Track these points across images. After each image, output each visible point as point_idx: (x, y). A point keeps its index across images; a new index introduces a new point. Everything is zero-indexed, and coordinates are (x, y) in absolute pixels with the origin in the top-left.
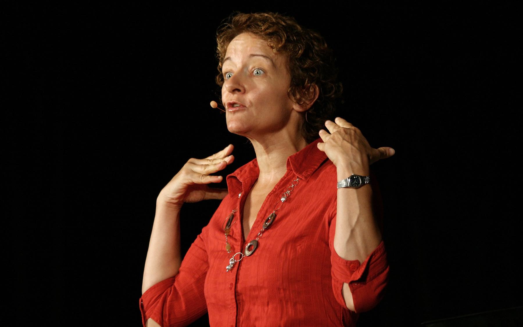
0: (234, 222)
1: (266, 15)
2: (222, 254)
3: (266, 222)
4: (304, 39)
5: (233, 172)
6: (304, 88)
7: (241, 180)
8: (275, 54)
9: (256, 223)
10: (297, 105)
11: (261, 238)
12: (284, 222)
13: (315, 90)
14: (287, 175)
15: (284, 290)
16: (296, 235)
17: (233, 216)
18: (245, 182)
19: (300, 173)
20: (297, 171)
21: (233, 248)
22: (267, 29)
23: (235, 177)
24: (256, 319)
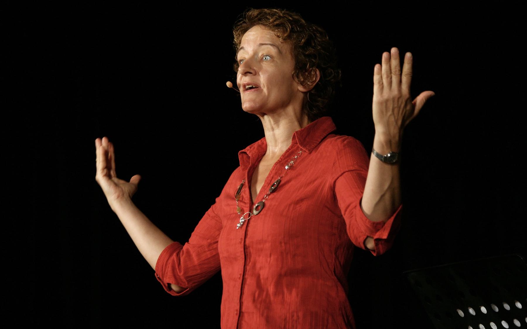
0: (243, 190)
1: (275, 10)
2: (234, 215)
4: (307, 31)
5: (245, 148)
6: (306, 71)
8: (282, 43)
9: (264, 188)
10: (302, 86)
11: (266, 200)
12: (287, 187)
13: (316, 73)
14: (292, 147)
15: (285, 243)
16: (298, 198)
17: (242, 185)
19: (305, 146)
20: (301, 144)
21: (242, 211)
22: (275, 21)
23: (245, 153)
24: (261, 268)
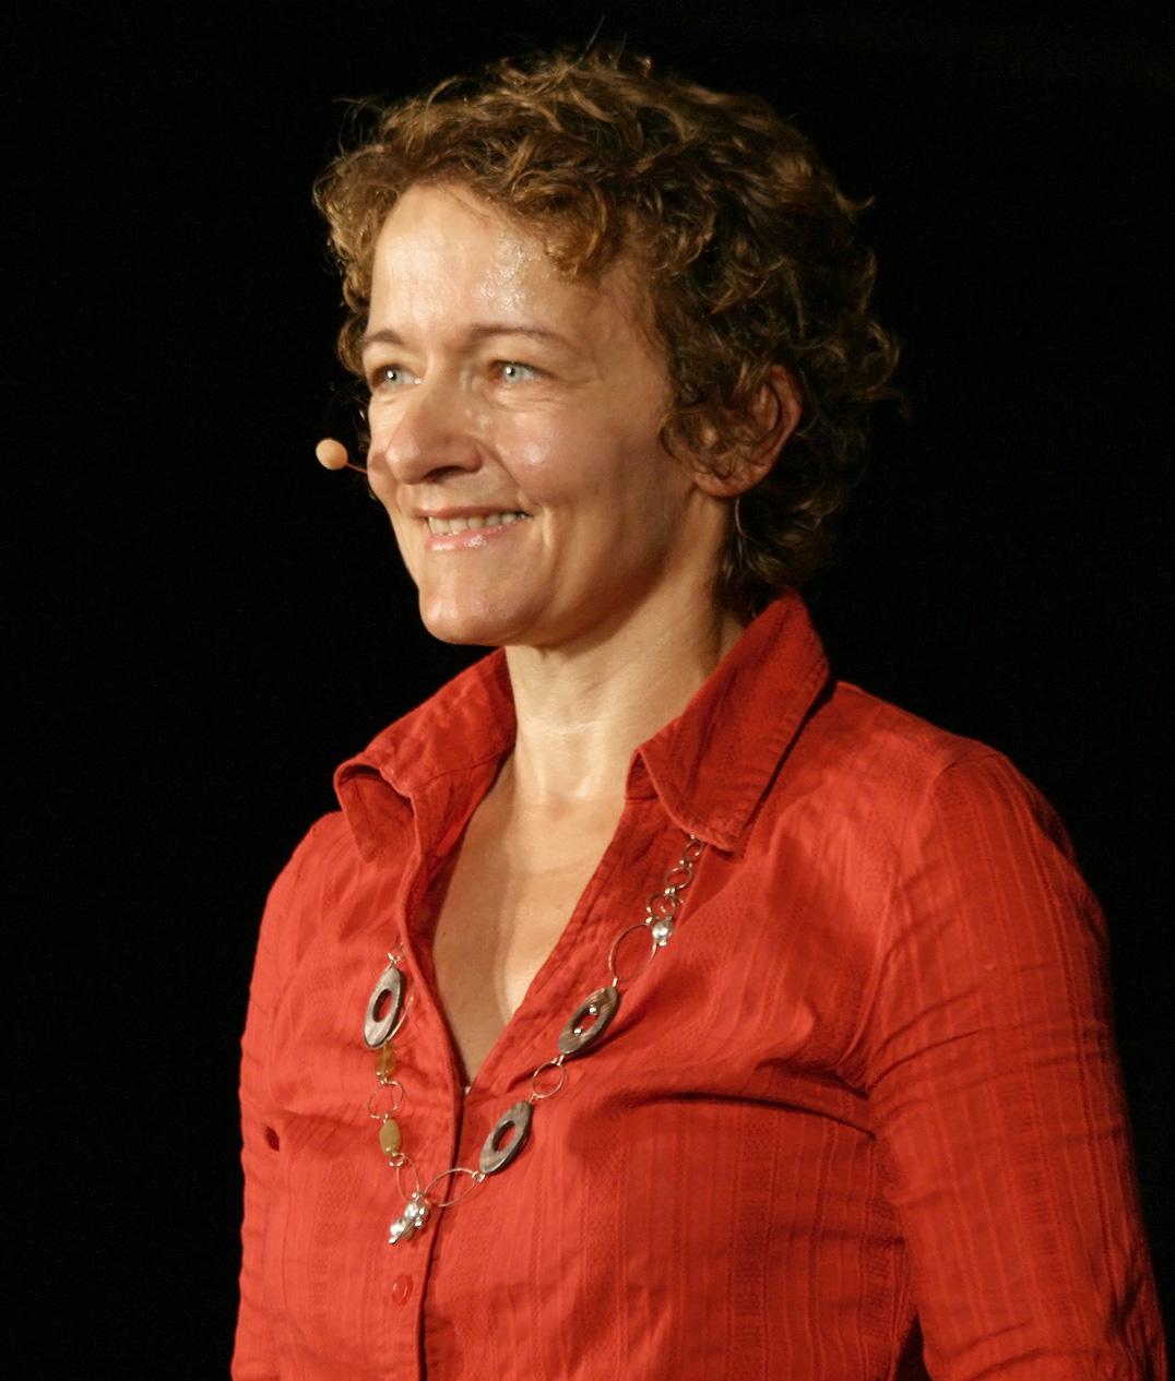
3: (576, 1024)
5: (362, 747)
7: (404, 788)
18: (423, 799)
23: (370, 772)
